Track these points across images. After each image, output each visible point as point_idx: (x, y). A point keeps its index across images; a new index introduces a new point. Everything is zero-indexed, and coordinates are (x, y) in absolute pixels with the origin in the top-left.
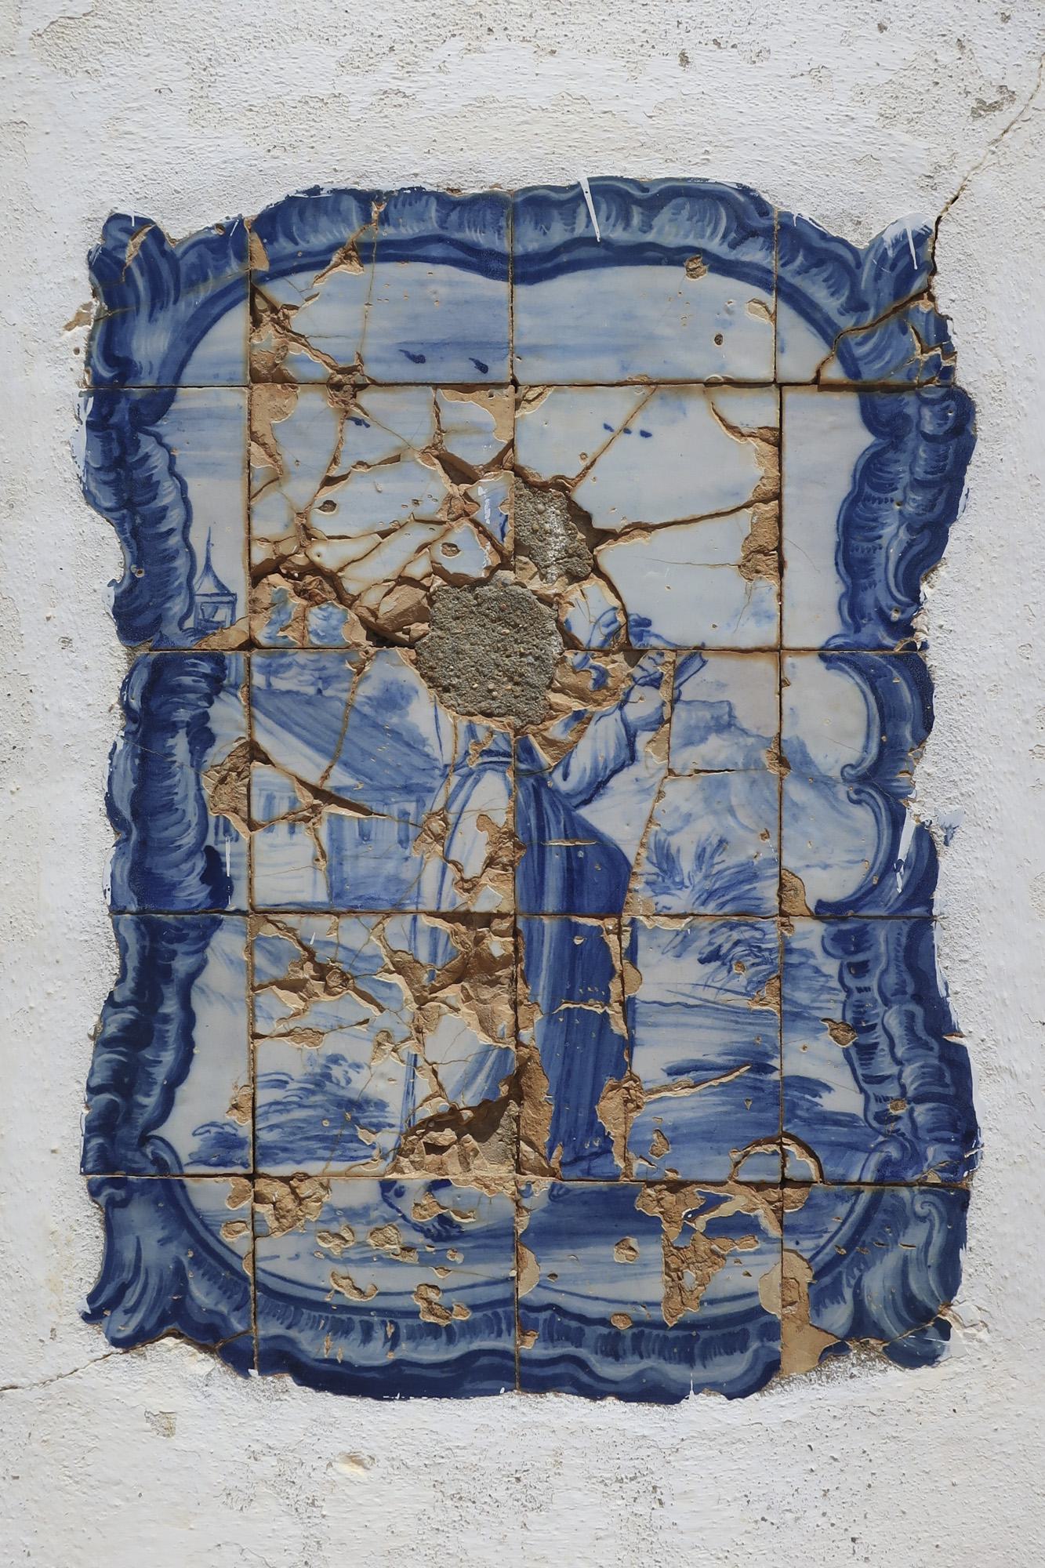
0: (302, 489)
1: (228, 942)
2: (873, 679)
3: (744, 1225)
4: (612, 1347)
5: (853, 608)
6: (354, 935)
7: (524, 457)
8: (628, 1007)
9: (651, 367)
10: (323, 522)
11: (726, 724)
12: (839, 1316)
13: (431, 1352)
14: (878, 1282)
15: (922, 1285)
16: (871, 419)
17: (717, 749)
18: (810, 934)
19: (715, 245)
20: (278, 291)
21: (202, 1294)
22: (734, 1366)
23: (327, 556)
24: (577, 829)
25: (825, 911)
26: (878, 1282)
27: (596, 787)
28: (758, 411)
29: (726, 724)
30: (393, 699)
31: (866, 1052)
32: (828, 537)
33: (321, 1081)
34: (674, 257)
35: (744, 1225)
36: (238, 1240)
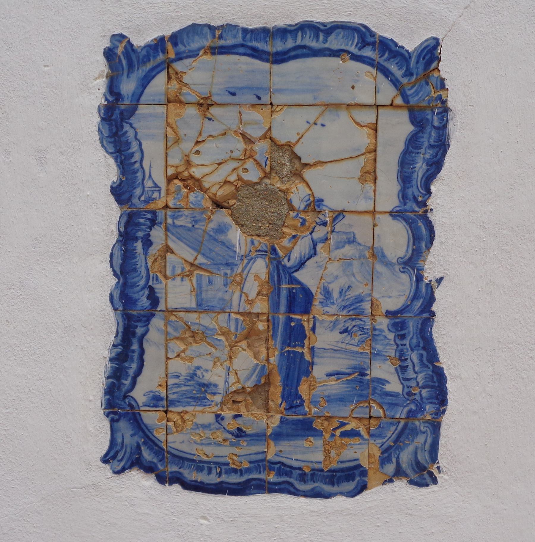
0: (187, 146)
1: (157, 323)
2: (411, 224)
3: (354, 434)
4: (303, 477)
5: (404, 196)
6: (206, 320)
7: (275, 134)
8: (312, 350)
9: (325, 98)
10: (195, 159)
11: (352, 241)
12: (390, 468)
13: (234, 479)
14: (406, 457)
15: (423, 457)
16: (413, 120)
17: (348, 250)
18: (383, 323)
19: (353, 49)
20: (178, 66)
21: (147, 455)
22: (351, 486)
23: (196, 172)
24: (293, 280)
25: (389, 314)
26: (406, 457)
27: (301, 264)
28: (368, 117)
29: (352, 241)
30: (222, 229)
31: (404, 369)
32: (394, 167)
33: (192, 376)
34: (336, 53)
35: (354, 434)
36: (160, 435)
